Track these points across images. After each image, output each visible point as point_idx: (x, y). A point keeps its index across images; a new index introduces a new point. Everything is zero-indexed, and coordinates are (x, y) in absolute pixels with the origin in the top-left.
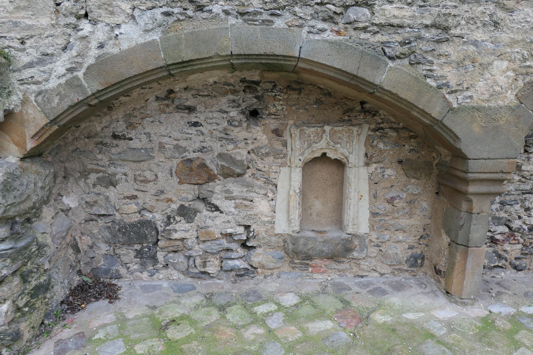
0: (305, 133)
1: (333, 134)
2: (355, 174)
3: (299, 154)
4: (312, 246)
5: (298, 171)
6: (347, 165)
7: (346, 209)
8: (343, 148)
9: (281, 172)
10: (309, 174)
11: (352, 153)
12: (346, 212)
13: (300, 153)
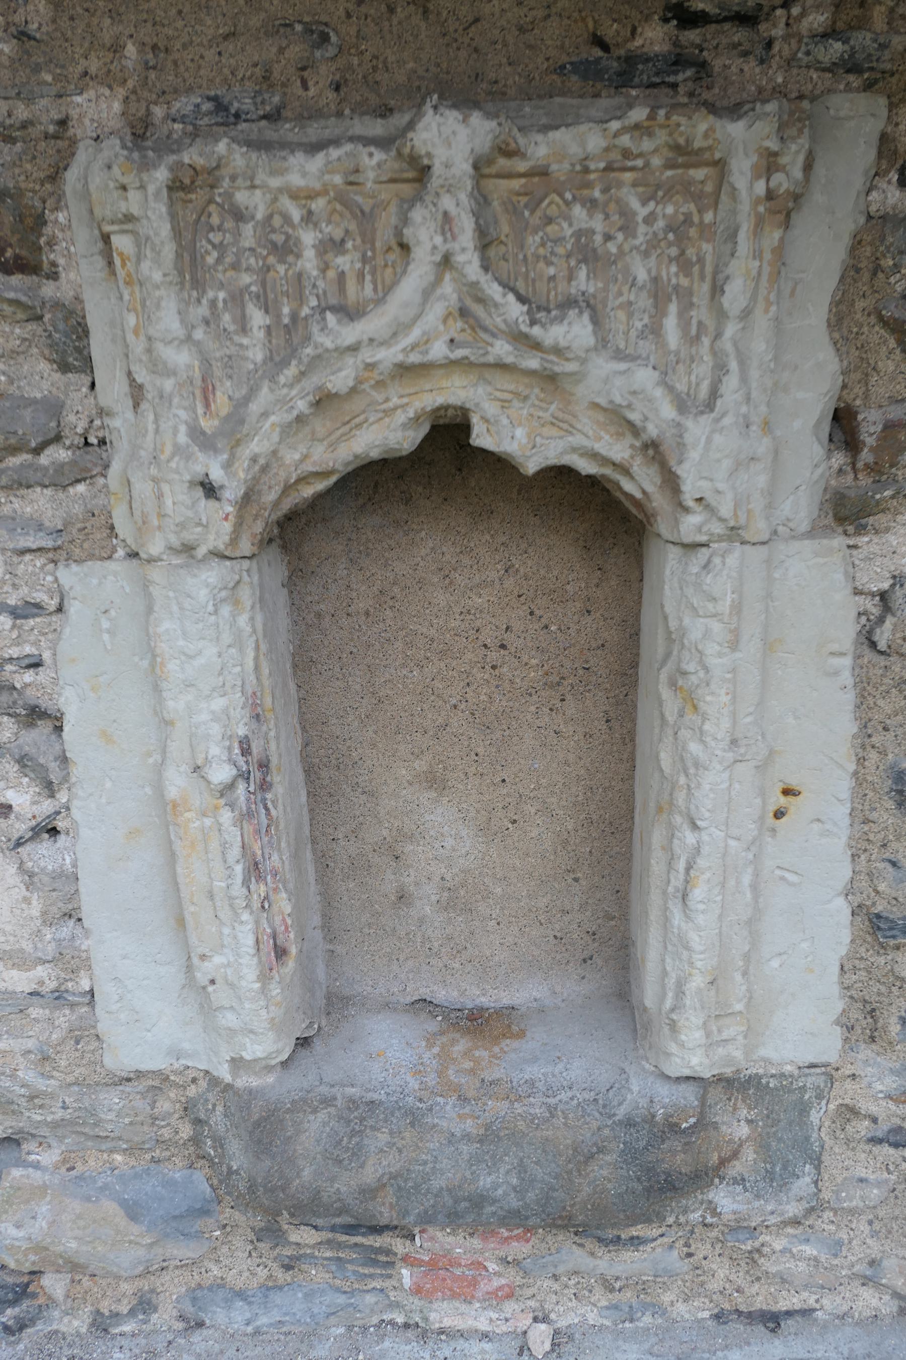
0: (239, 215)
1: (513, 210)
2: (737, 608)
3: (196, 433)
4: (392, 1162)
5: (203, 594)
6: (663, 527)
7: (655, 899)
8: (619, 355)
9: (73, 608)
10: (361, 605)
11: (710, 405)
12: (654, 914)
13: (208, 425)
